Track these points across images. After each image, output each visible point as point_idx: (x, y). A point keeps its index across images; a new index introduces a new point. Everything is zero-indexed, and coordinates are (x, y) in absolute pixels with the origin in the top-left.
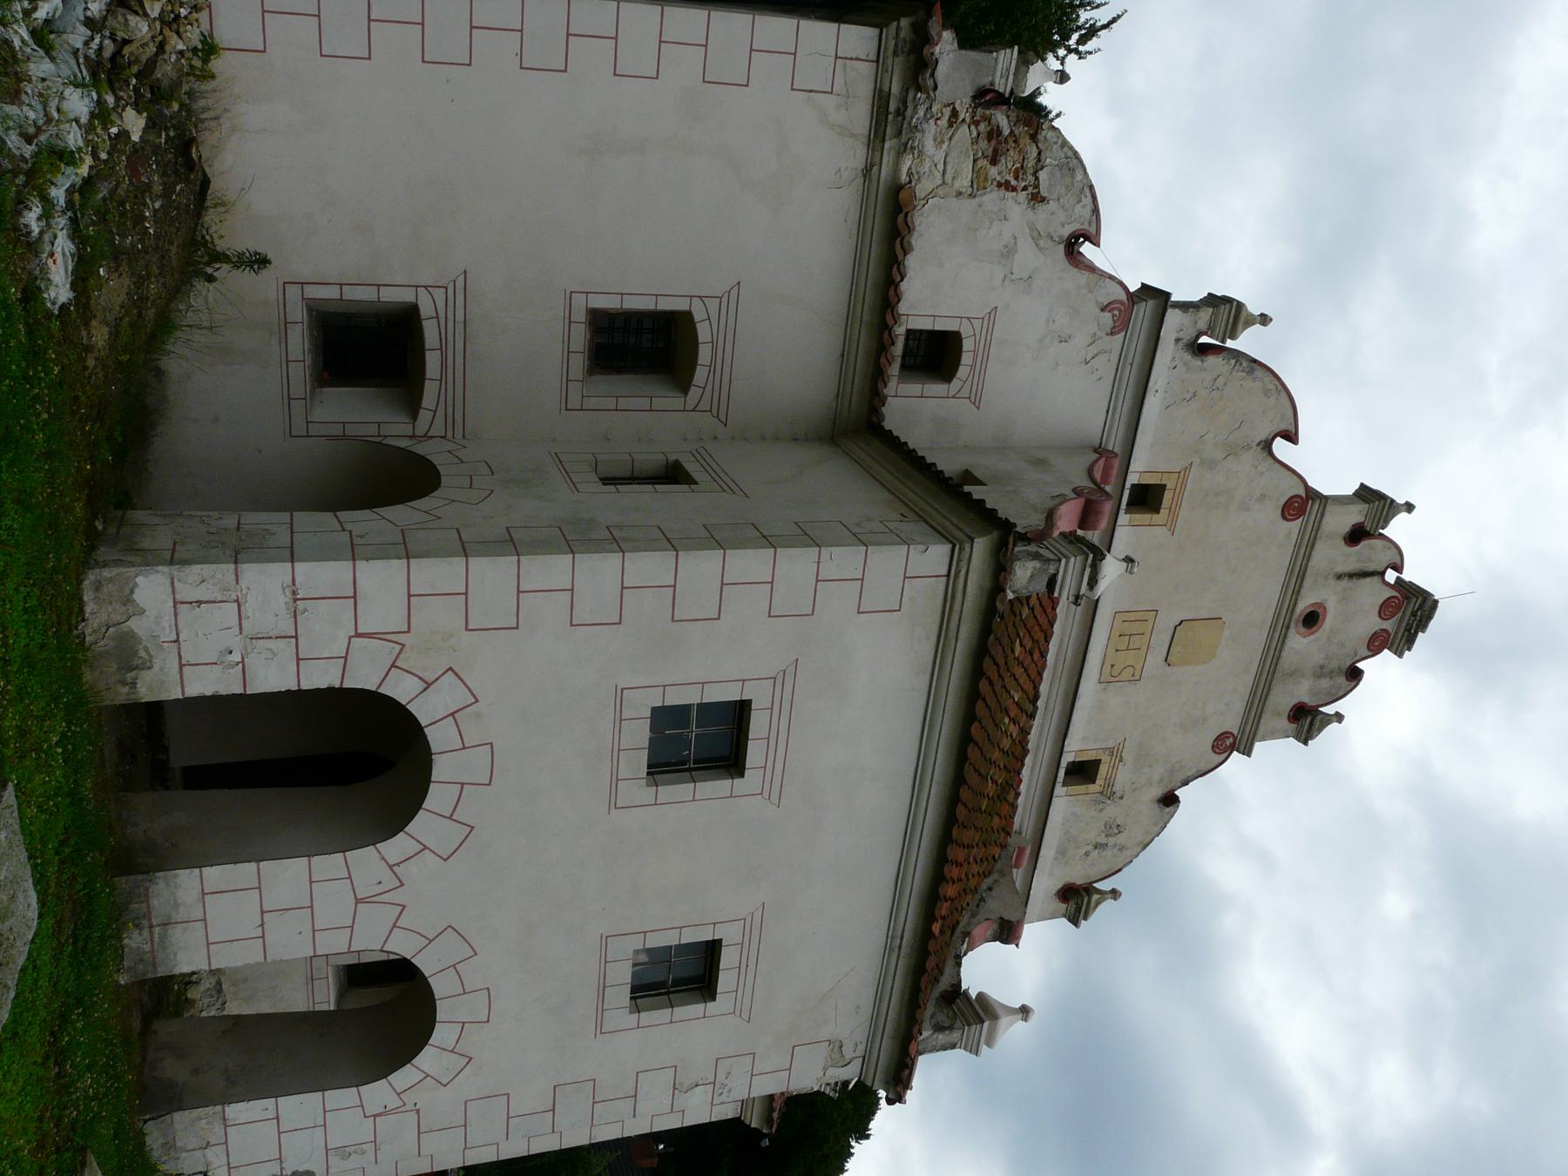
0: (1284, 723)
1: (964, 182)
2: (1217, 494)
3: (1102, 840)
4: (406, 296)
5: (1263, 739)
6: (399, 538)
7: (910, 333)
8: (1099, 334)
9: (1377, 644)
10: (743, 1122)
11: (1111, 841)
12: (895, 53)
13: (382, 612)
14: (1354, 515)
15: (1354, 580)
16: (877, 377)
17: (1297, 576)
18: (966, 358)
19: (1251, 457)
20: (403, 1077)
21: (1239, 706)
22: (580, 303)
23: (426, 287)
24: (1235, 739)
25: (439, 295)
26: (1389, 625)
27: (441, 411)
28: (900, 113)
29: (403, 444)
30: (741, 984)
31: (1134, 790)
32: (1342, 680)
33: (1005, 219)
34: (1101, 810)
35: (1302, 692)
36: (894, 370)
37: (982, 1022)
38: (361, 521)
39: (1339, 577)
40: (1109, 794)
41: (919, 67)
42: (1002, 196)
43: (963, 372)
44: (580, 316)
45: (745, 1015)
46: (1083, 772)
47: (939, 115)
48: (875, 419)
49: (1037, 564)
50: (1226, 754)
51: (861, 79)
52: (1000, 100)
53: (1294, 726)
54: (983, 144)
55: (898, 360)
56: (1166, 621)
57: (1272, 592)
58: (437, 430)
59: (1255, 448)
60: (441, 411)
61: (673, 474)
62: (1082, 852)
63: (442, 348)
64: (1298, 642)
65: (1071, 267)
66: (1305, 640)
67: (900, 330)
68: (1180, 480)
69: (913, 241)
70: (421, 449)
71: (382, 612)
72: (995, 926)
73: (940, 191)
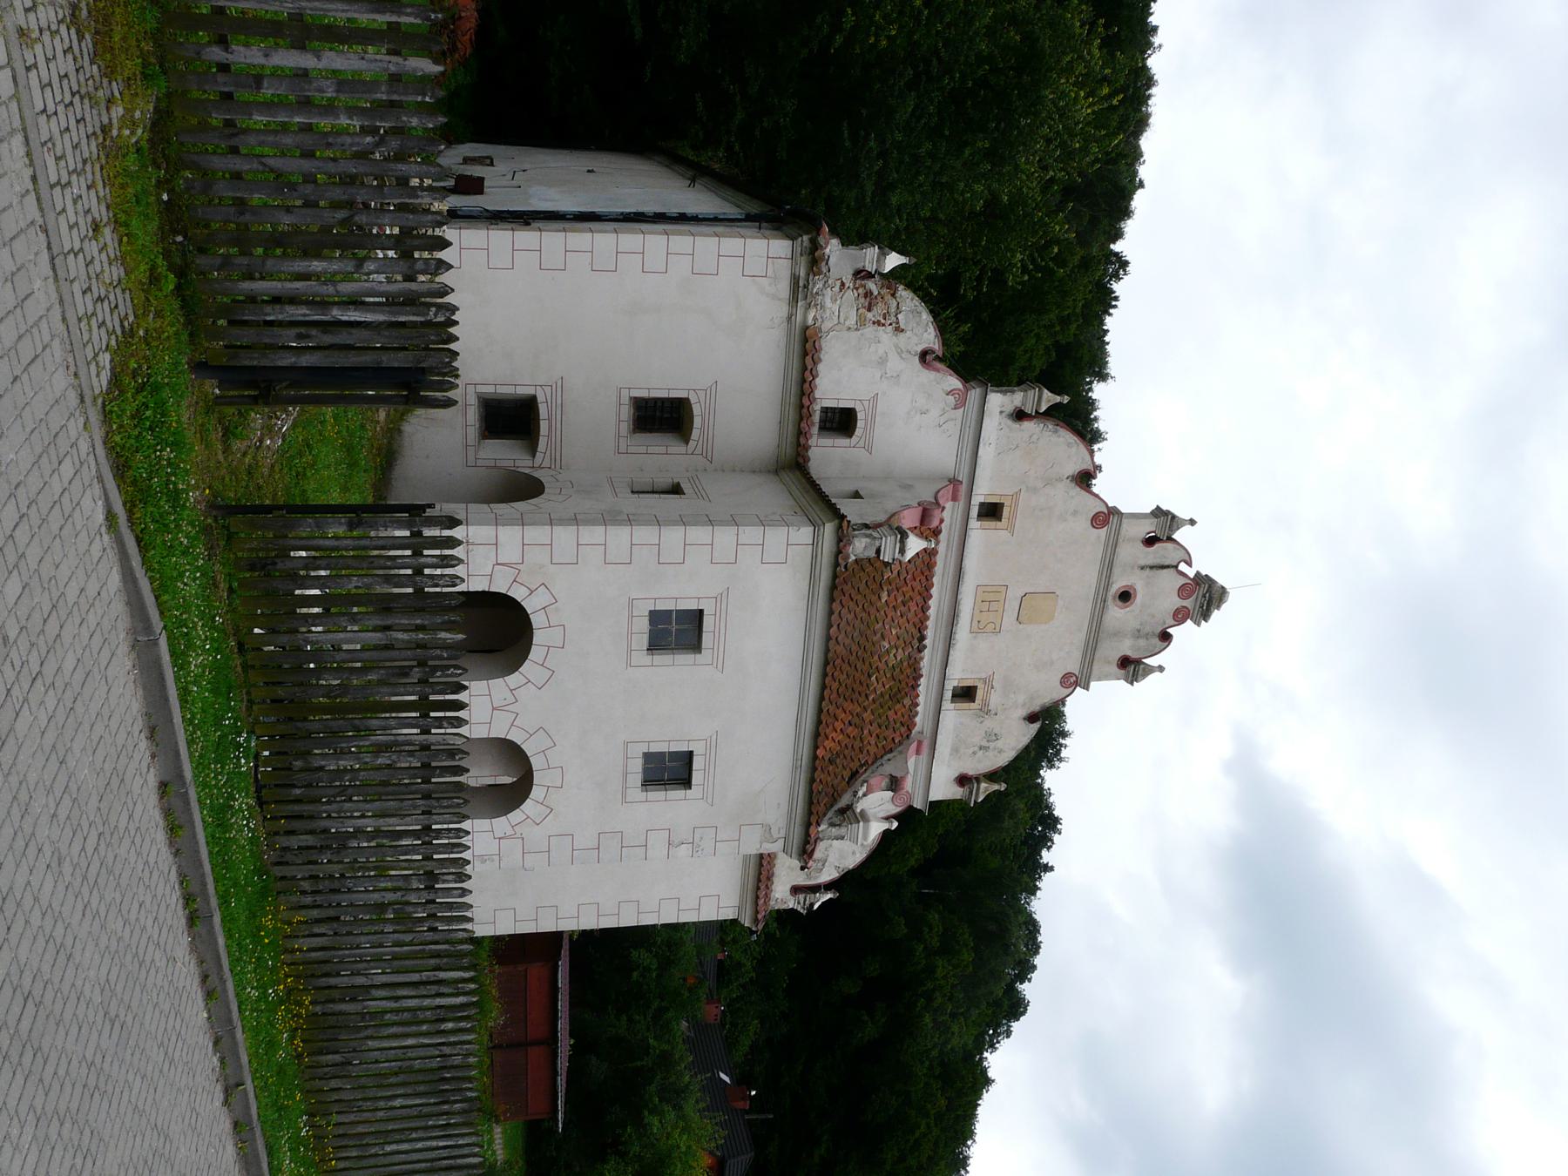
0: (1114, 669)
1: (852, 321)
2: (1041, 510)
3: (984, 743)
4: (529, 391)
5: (1099, 679)
6: (519, 516)
7: (825, 410)
8: (947, 409)
9: (1180, 616)
10: (740, 923)
11: (992, 745)
12: (801, 255)
13: (510, 553)
14: (1148, 528)
15: (1154, 570)
16: (800, 435)
17: (1108, 567)
18: (860, 424)
20: (515, 816)
21: (1077, 655)
22: (625, 394)
24: (1077, 678)
25: (548, 390)
26: (1188, 603)
27: (548, 453)
28: (805, 287)
29: (527, 471)
31: (1005, 709)
32: (1156, 641)
33: (879, 342)
34: (982, 722)
35: (1127, 648)
36: (815, 430)
37: (859, 822)
38: (502, 509)
39: (1142, 568)
40: (985, 711)
41: (815, 261)
43: (858, 432)
44: (626, 400)
45: (710, 800)
46: (966, 694)
48: (801, 461)
49: (868, 540)
50: (1071, 689)
51: (783, 269)
52: (870, 276)
53: (1123, 671)
54: (862, 300)
55: (817, 425)
56: (1015, 593)
57: (1091, 577)
58: (546, 463)
60: (548, 453)
61: (676, 490)
64: (1116, 614)
67: (817, 407)
70: (536, 474)
71: (510, 553)
72: (887, 780)
73: (837, 328)
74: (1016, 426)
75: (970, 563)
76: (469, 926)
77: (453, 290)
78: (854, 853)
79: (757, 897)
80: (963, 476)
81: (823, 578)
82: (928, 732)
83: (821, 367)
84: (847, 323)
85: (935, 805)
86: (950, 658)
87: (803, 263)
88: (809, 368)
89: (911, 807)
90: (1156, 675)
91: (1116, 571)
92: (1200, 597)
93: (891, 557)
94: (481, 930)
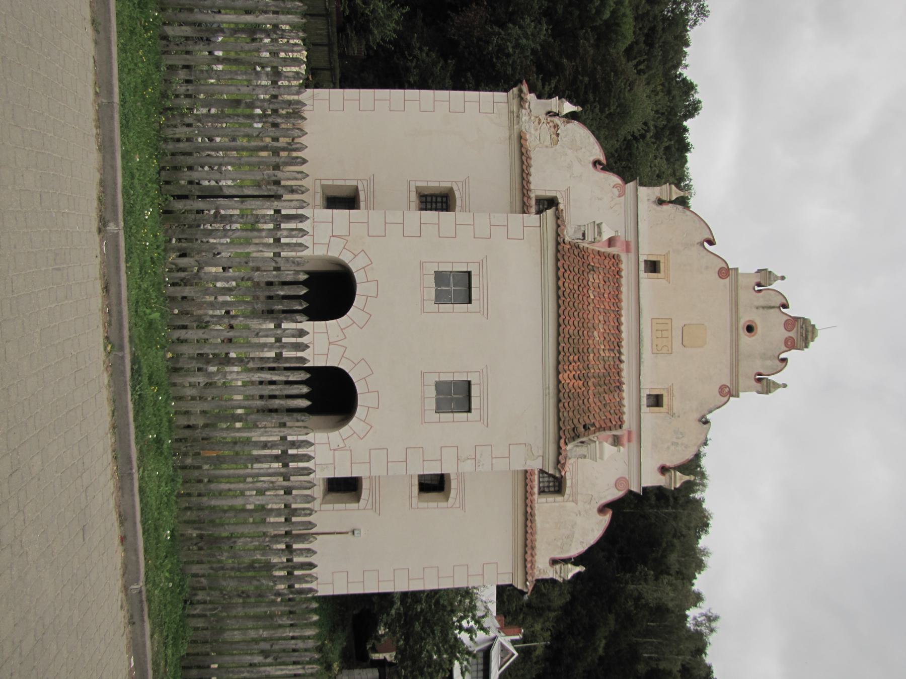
3: (675, 440)
5: (745, 391)
12: (513, 99)
15: (765, 309)
21: (727, 371)
24: (729, 389)
25: (365, 183)
35: (758, 366)
36: (536, 490)
37: (595, 442)
39: (757, 308)
41: (521, 99)
46: (656, 401)
51: (504, 108)
52: (556, 115)
54: (552, 129)
67: (533, 195)
74: (659, 208)
76: (313, 585)
77: (307, 147)
78: (593, 530)
79: (525, 560)
81: (550, 247)
82: (634, 429)
84: (546, 143)
85: (645, 489)
86: (641, 327)
87: (515, 102)
88: (529, 491)
89: (630, 492)
91: (741, 309)
92: (799, 328)
93: (593, 237)
94: (324, 589)
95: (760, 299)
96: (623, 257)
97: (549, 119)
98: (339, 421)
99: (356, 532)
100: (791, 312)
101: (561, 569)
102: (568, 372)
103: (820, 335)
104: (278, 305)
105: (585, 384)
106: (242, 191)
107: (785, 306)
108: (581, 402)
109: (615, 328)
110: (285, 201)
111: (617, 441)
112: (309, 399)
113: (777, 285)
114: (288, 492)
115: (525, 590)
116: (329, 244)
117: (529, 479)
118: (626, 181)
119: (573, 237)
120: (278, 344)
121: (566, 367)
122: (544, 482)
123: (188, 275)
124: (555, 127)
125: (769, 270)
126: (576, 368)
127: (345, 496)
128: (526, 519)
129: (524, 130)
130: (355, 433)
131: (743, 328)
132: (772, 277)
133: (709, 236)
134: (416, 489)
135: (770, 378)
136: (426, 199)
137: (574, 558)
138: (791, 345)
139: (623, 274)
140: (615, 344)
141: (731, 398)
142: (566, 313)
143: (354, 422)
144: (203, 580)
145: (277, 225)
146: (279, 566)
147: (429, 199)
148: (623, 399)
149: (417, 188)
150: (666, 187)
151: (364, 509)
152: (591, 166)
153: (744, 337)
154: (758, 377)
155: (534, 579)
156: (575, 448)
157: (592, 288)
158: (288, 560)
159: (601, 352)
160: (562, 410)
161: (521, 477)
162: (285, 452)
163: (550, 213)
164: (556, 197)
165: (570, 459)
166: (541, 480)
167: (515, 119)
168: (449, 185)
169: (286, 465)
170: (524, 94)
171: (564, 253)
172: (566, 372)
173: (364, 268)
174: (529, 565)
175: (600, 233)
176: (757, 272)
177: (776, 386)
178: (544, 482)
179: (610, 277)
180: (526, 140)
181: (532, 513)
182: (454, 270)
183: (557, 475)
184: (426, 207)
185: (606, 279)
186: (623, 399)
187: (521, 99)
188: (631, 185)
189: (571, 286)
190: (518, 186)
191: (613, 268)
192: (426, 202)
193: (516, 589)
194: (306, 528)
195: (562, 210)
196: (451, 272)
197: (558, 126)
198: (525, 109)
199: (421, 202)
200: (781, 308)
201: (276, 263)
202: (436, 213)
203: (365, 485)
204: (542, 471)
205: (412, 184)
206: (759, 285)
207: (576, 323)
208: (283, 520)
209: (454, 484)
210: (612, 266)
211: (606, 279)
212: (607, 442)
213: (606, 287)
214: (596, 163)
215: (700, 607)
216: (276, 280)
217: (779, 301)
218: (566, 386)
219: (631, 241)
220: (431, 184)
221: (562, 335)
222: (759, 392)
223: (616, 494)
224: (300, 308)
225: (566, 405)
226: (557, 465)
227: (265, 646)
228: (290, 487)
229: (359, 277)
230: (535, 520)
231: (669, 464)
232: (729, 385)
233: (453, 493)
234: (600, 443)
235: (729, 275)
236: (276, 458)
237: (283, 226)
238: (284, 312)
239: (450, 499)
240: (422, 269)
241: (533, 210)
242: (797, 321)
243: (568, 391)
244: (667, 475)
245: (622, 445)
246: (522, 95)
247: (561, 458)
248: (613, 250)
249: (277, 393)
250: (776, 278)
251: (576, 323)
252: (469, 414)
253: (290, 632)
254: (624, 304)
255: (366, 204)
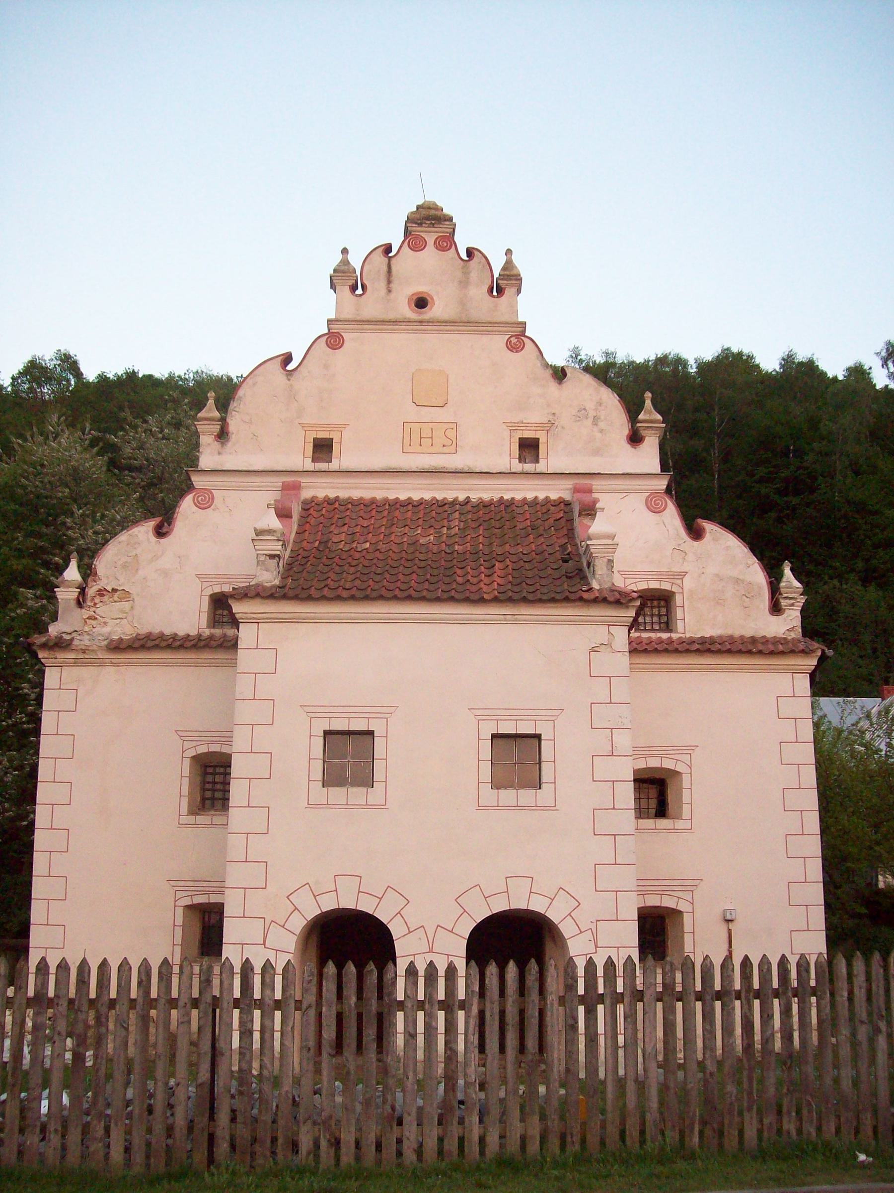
11: (592, 413)
19: (301, 384)
22: (184, 819)
23: (175, 901)
24: (512, 336)
30: (529, 718)
34: (563, 428)
35: (478, 292)
36: (665, 636)
37: (588, 545)
39: (390, 291)
40: (549, 426)
41: (61, 644)
42: (270, 504)
47: (91, 626)
51: (70, 673)
52: (83, 591)
54: (106, 598)
59: (291, 381)
62: (599, 435)
63: (208, 893)
64: (437, 310)
65: (173, 533)
66: (437, 303)
67: (207, 632)
68: (311, 429)
69: (157, 632)
74: (233, 438)
75: (378, 463)
78: (727, 548)
80: (277, 482)
82: (569, 483)
83: (168, 631)
85: (664, 467)
86: (414, 469)
87: (62, 656)
89: (668, 491)
90: (515, 259)
91: (392, 316)
95: (376, 287)
96: (306, 494)
97: (89, 603)
98: (554, 941)
99: (729, 917)
100: (396, 239)
101: (786, 598)
102: (482, 585)
103: (433, 197)
104: (371, 1005)
105: (500, 558)
106: (205, 1053)
107: (388, 249)
108: (527, 566)
109: (416, 509)
110: (221, 992)
111: (590, 511)
112: (507, 963)
113: (356, 261)
114: (639, 996)
115: (819, 653)
116: (277, 950)
117: (646, 647)
118: (189, 487)
119: (275, 573)
120: (427, 1006)
121: (474, 589)
122: (652, 623)
123: (325, 1137)
124: (102, 595)
125: (332, 272)
126: (475, 573)
127: (671, 931)
128: (709, 651)
129: (105, 643)
130: (570, 914)
131: (421, 313)
132: (343, 268)
133: (277, 364)
134: (662, 823)
135: (496, 275)
136: (208, 799)
137: (770, 578)
138: (447, 242)
139: (332, 495)
140: (440, 510)
141: (526, 334)
142: (392, 586)
143: (554, 915)
144: (766, 1121)
145: (255, 1003)
146: (747, 1011)
147: (208, 794)
148: (525, 499)
149: (191, 812)
150: (201, 427)
151: (693, 904)
152: (163, 541)
153: (436, 310)
154: (495, 293)
155: (802, 639)
156: (597, 576)
157: (354, 546)
158: (738, 997)
159: (453, 532)
160: (539, 596)
161: (642, 659)
162: (582, 1000)
163: (237, 608)
164: (211, 596)
165: (613, 584)
166: (650, 628)
167: (87, 657)
168: (187, 763)
169: (601, 999)
170: (48, 640)
171: (300, 587)
172: (481, 588)
173: (315, 896)
174: (781, 647)
175: (270, 532)
176: (335, 292)
177: (509, 265)
178: (652, 623)
179: (337, 516)
180: (121, 639)
181: (700, 642)
182: (321, 757)
183: (638, 603)
184: (220, 799)
185: (340, 523)
186: (525, 499)
187: (61, 644)
188: (197, 480)
189: (351, 577)
190: (191, 656)
191: (324, 512)
192: (213, 799)
193: (817, 667)
194: (691, 970)
195: (234, 589)
196: (324, 762)
197: (100, 590)
198: (72, 639)
199: (213, 806)
200: (390, 255)
201: (310, 1006)
202: (233, 783)
203: (653, 901)
204: (634, 625)
205: (184, 819)
206: (354, 288)
207: (407, 571)
208: (679, 1005)
209: (654, 763)
210: (320, 513)
211: (340, 523)
212: (590, 527)
213: (353, 523)
214: (160, 533)
215: (870, 368)
216: (334, 1008)
217: (380, 260)
218: (502, 589)
219: (283, 483)
220: (185, 790)
221: (425, 593)
222: (519, 291)
223: (671, 515)
224: (375, 973)
225: (532, 589)
226: (621, 603)
227: (863, 1032)
228: (633, 993)
229: (329, 904)
230: (711, 638)
231: (626, 431)
232: (508, 337)
233: (668, 764)
234: (589, 539)
235: (338, 333)
236: (591, 1013)
237: (257, 995)
238: (380, 997)
239: (678, 769)
240: (318, 806)
241: (230, 632)
242: (410, 233)
243: (509, 586)
244: (643, 433)
245: (595, 502)
246: (51, 644)
247: (611, 599)
248: (296, 511)
249: (497, 1011)
250: (345, 262)
251: (407, 571)
252: (543, 737)
253: (842, 996)
254: (379, 495)
255: (214, 892)
